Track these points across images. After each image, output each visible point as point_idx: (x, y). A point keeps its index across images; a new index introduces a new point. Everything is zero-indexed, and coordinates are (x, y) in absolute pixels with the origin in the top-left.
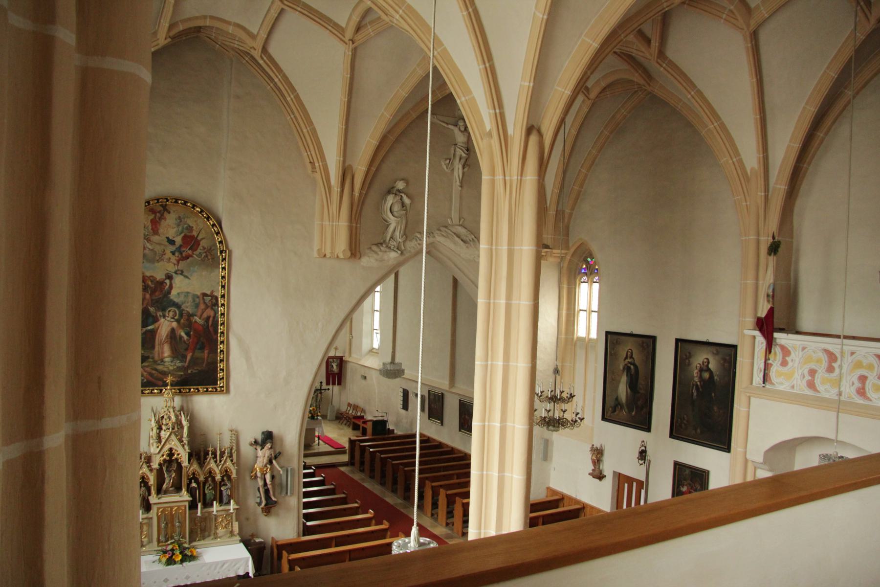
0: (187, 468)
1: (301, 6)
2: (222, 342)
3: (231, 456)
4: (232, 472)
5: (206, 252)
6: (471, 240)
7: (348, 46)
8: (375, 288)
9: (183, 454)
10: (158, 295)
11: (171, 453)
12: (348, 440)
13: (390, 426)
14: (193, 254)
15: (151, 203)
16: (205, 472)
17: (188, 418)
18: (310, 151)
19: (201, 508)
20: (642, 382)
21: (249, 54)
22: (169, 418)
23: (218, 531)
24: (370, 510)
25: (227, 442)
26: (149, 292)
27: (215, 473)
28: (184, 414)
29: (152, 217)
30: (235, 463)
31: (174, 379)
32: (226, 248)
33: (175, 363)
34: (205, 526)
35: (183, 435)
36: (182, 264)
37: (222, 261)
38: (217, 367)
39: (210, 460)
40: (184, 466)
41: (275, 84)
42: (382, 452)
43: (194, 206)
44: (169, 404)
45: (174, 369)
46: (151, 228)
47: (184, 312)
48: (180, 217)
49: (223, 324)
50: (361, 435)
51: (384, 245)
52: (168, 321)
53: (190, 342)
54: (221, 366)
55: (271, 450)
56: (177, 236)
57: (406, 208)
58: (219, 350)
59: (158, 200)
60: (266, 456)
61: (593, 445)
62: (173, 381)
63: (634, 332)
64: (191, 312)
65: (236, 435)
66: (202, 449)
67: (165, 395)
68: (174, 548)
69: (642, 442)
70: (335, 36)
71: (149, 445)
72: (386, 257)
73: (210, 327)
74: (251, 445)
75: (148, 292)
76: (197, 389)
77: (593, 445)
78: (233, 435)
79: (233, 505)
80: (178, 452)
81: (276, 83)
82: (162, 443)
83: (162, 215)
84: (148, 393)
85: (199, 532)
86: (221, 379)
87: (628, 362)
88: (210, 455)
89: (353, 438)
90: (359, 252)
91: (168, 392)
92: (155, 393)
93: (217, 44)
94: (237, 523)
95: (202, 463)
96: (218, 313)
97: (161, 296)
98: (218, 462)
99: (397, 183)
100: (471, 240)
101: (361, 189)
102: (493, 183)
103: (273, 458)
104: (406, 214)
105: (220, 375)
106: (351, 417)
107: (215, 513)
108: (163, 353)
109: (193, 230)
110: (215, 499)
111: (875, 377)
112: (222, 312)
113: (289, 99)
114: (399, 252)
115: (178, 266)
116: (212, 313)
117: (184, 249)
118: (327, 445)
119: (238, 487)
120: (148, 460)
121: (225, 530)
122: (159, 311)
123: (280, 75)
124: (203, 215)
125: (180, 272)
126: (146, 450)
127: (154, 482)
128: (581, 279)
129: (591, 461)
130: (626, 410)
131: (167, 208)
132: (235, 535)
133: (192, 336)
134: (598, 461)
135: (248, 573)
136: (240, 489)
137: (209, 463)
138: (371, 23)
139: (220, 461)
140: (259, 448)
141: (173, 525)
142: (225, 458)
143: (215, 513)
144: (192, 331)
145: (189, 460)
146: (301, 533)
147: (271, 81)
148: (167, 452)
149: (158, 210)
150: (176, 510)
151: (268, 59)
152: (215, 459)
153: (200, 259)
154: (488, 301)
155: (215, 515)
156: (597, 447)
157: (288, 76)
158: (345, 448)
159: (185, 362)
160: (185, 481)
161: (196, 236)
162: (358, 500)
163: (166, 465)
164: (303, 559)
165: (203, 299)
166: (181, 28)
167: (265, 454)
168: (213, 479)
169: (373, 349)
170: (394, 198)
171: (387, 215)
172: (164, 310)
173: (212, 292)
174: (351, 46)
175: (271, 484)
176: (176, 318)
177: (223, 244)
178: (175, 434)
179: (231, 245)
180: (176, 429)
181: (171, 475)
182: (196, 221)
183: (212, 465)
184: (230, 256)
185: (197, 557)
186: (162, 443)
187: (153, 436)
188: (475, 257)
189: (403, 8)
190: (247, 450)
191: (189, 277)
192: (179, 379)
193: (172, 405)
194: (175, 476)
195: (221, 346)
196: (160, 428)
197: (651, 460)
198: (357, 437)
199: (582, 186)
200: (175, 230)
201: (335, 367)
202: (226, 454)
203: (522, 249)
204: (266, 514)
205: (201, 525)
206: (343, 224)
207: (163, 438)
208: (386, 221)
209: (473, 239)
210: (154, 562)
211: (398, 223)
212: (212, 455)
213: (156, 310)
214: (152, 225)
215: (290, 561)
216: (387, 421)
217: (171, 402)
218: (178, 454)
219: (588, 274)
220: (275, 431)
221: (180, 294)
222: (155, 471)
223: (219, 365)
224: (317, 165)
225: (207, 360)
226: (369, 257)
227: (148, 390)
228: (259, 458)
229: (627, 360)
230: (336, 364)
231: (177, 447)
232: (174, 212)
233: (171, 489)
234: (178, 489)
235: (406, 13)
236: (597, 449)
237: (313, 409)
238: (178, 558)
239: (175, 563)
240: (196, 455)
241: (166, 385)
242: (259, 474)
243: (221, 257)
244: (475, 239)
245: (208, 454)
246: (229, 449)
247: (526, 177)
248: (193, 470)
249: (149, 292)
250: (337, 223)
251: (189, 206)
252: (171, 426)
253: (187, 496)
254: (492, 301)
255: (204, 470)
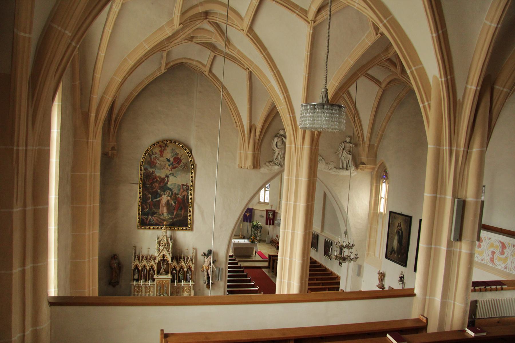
2: (190, 207)
3: (192, 260)
4: (192, 268)
5: (184, 165)
6: (320, 159)
9: (169, 258)
11: (164, 256)
14: (178, 166)
15: (160, 142)
20: (404, 241)
23: (184, 294)
24: (262, 292)
27: (184, 267)
29: (160, 149)
32: (194, 163)
33: (169, 215)
36: (173, 171)
39: (182, 261)
43: (179, 144)
45: (168, 218)
47: (173, 193)
48: (173, 149)
52: (166, 196)
54: (190, 218)
58: (189, 211)
59: (163, 141)
60: (209, 261)
61: (379, 271)
63: (403, 213)
64: (176, 193)
65: (195, 250)
69: (401, 272)
72: (273, 168)
76: (178, 228)
77: (379, 271)
82: (160, 252)
83: (165, 148)
85: (175, 293)
86: (189, 224)
87: (399, 228)
90: (259, 166)
94: (193, 291)
98: (186, 262)
99: (280, 131)
100: (320, 159)
102: (290, 148)
105: (189, 222)
107: (183, 285)
108: (163, 211)
111: (498, 253)
116: (186, 193)
117: (174, 164)
118: (259, 257)
121: (188, 293)
122: (162, 192)
123: (218, 82)
125: (172, 174)
128: (383, 181)
129: (378, 279)
130: (396, 254)
134: (381, 280)
139: (187, 262)
140: (206, 257)
141: (163, 289)
142: (189, 261)
149: (163, 146)
150: (165, 282)
151: (212, 76)
154: (286, 202)
156: (382, 272)
161: (180, 158)
163: (162, 262)
165: (182, 187)
166: (172, 64)
168: (183, 270)
172: (164, 191)
173: (187, 184)
176: (170, 195)
179: (197, 161)
180: (166, 246)
182: (180, 151)
183: (183, 263)
184: (196, 167)
186: (160, 252)
188: (322, 168)
189: (253, 66)
190: (200, 257)
192: (170, 223)
194: (166, 267)
195: (190, 209)
196: (160, 245)
197: (406, 282)
199: (383, 131)
201: (271, 215)
203: (302, 180)
206: (250, 153)
208: (274, 150)
209: (321, 159)
212: (183, 259)
213: (161, 191)
214: (160, 153)
218: (167, 257)
219: (386, 179)
222: (157, 264)
226: (264, 168)
228: (205, 262)
229: (398, 228)
232: (170, 146)
233: (164, 272)
235: (254, 69)
236: (381, 273)
237: (253, 238)
241: (164, 226)
242: (205, 270)
244: (322, 159)
245: (181, 258)
247: (305, 146)
248: (174, 265)
249: (158, 183)
254: (288, 202)
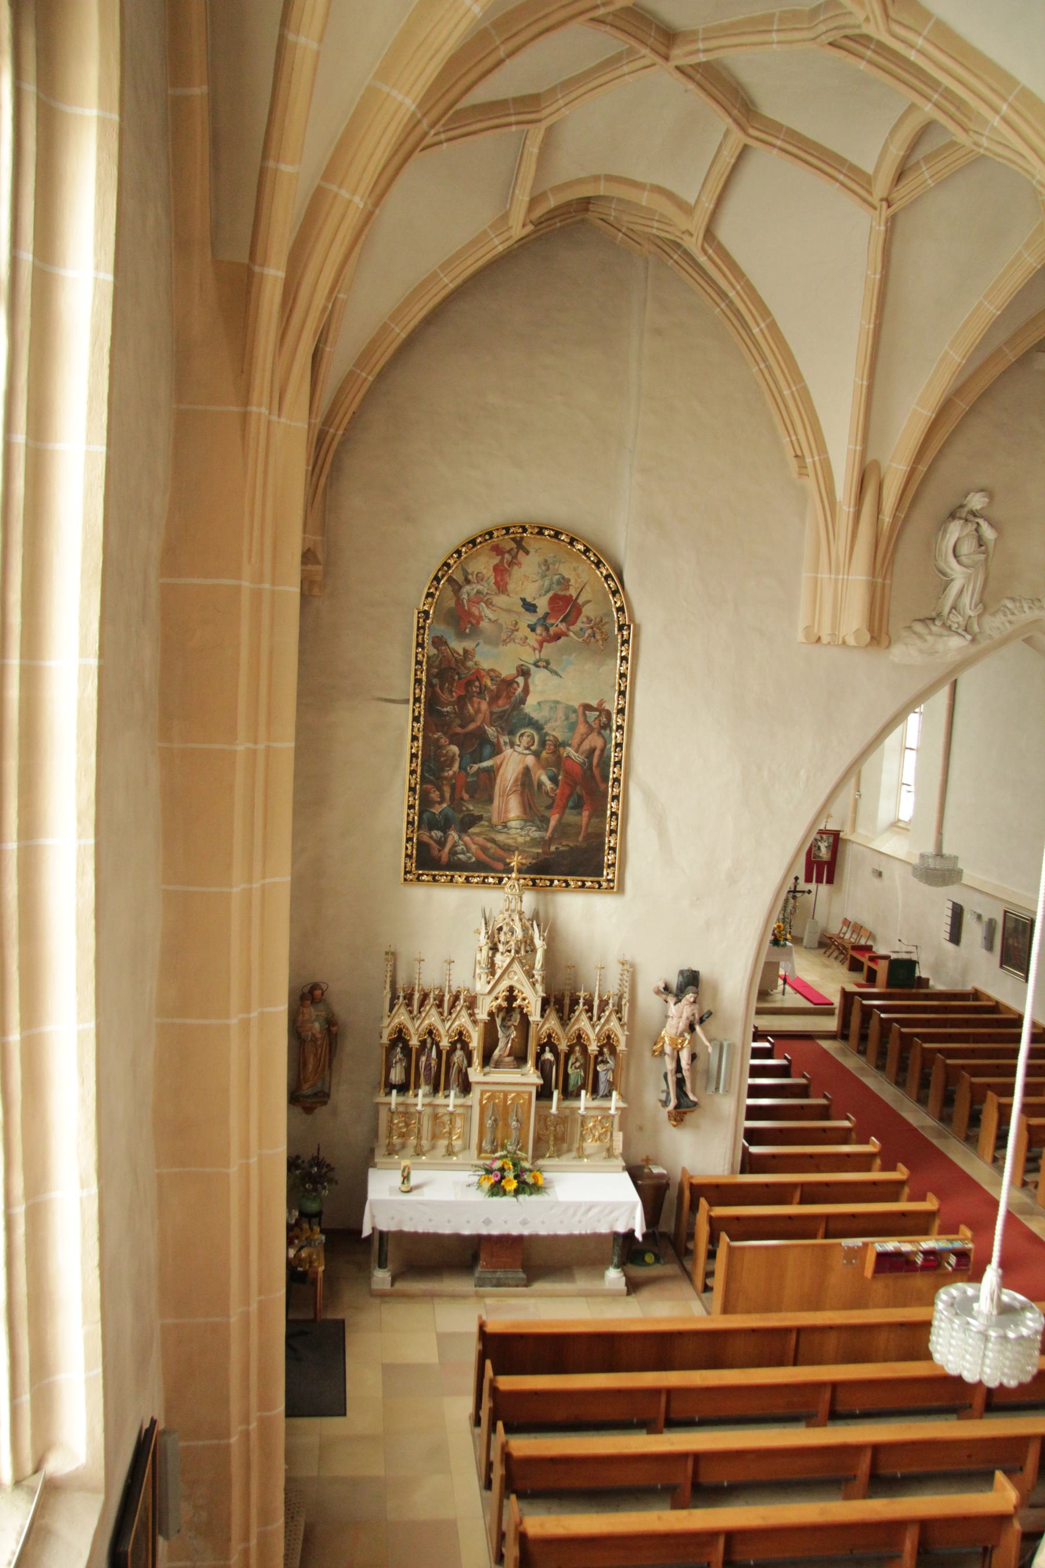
0: (538, 1025)
1: (782, 137)
2: (615, 798)
3: (619, 1011)
4: (618, 1041)
5: (592, 628)
7: (878, 212)
8: (915, 709)
9: (531, 999)
10: (502, 705)
11: (511, 995)
12: (839, 989)
13: (922, 972)
14: (568, 629)
15: (495, 534)
16: (570, 1034)
17: (546, 934)
18: (796, 434)
19: (559, 1100)
21: (678, 245)
22: (512, 931)
24: (873, 1138)
25: (613, 985)
26: (487, 699)
27: (589, 1039)
28: (538, 925)
29: (496, 560)
30: (625, 1024)
31: (524, 861)
32: (630, 620)
34: (563, 1133)
35: (534, 964)
37: (622, 645)
38: (603, 844)
40: (534, 1022)
41: (731, 304)
42: (903, 1023)
44: (512, 906)
45: (525, 842)
46: (494, 581)
47: (547, 738)
48: (546, 561)
49: (618, 763)
50: (864, 982)
51: (938, 623)
52: (519, 753)
53: (556, 795)
54: (611, 841)
55: (692, 1007)
56: (540, 596)
57: (987, 548)
58: (609, 813)
59: (507, 529)
60: (685, 1015)
62: (522, 864)
65: (631, 971)
66: (567, 993)
67: (507, 890)
68: (506, 1167)
70: (851, 194)
71: (474, 977)
73: (594, 768)
74: (658, 992)
75: (485, 699)
76: (566, 881)
78: (626, 973)
79: (617, 1101)
80: (524, 995)
81: (731, 302)
82: (497, 977)
83: (515, 557)
84: (477, 883)
85: (551, 1143)
86: (609, 866)
88: (581, 1005)
89: (852, 988)
90: (887, 634)
91: (512, 881)
92: (490, 884)
93: (620, 231)
95: (566, 1017)
96: (611, 743)
97: (507, 707)
98: (595, 1018)
99: (970, 497)
101: (896, 510)
103: (696, 1022)
104: (986, 560)
105: (609, 858)
106: (848, 946)
107: (582, 1111)
108: (506, 811)
109: (569, 586)
110: (583, 1086)
112: (618, 742)
113: (756, 331)
114: (969, 637)
115: (540, 652)
119: (628, 1065)
120: (472, 1004)
121: (598, 1143)
123: (739, 283)
124: (589, 558)
126: (468, 984)
127: (478, 1044)
131: (523, 544)
132: (616, 1157)
133: (560, 785)
135: (632, 1232)
136: (632, 1070)
137: (577, 1020)
138: (927, 159)
139: (599, 1018)
140: (671, 1000)
141: (507, 1125)
142: (607, 1013)
143: (582, 1111)
144: (561, 773)
145: (543, 1010)
146: (738, 1167)
147: (721, 298)
148: (504, 993)
149: (508, 548)
150: (513, 1099)
152: (590, 1014)
153: (581, 640)
155: (583, 1116)
157: (755, 285)
158: (832, 1004)
159: (546, 830)
160: (532, 1049)
161: (574, 598)
162: (851, 1114)
163: (501, 1015)
164: (738, 1218)
165: (585, 715)
166: (552, 202)
167: (682, 1013)
168: (584, 1049)
169: (899, 820)
170: (962, 530)
171: (946, 561)
172: (512, 733)
173: (601, 703)
174: (886, 212)
175: (688, 1070)
176: (533, 748)
177: (624, 612)
178: (521, 962)
180: (523, 952)
181: (509, 1035)
182: (575, 569)
185: (545, 1188)
186: (497, 977)
187: (482, 962)
190: (648, 1001)
191: (560, 672)
192: (534, 861)
193: (519, 909)
194: (516, 1037)
195: (614, 804)
196: (494, 949)
198: (859, 985)
200: (537, 584)
201: (823, 850)
202: (611, 1005)
204: (675, 1123)
205: (555, 1130)
207: (499, 967)
208: (944, 574)
210: (469, 1186)
211: (968, 579)
212: (584, 1004)
213: (498, 732)
214: (496, 578)
215: (711, 1220)
216: (918, 963)
217: (516, 903)
218: (524, 999)
220: (704, 971)
221: (542, 705)
222: (481, 1025)
223: (607, 839)
224: (809, 460)
225: (587, 828)
226: (906, 644)
227: (478, 876)
228: (669, 1020)
230: (826, 844)
231: (523, 985)
232: (536, 551)
233: (508, 1059)
234: (520, 1059)
238: (511, 1185)
239: (505, 1193)
240: (555, 1004)
241: (510, 870)
242: (668, 1049)
243: (619, 637)
245: (578, 1003)
246: (616, 998)
248: (548, 1029)
249: (487, 699)
250: (846, 577)
251: (563, 540)
252: (513, 946)
253: (535, 1075)
255: (569, 1031)
